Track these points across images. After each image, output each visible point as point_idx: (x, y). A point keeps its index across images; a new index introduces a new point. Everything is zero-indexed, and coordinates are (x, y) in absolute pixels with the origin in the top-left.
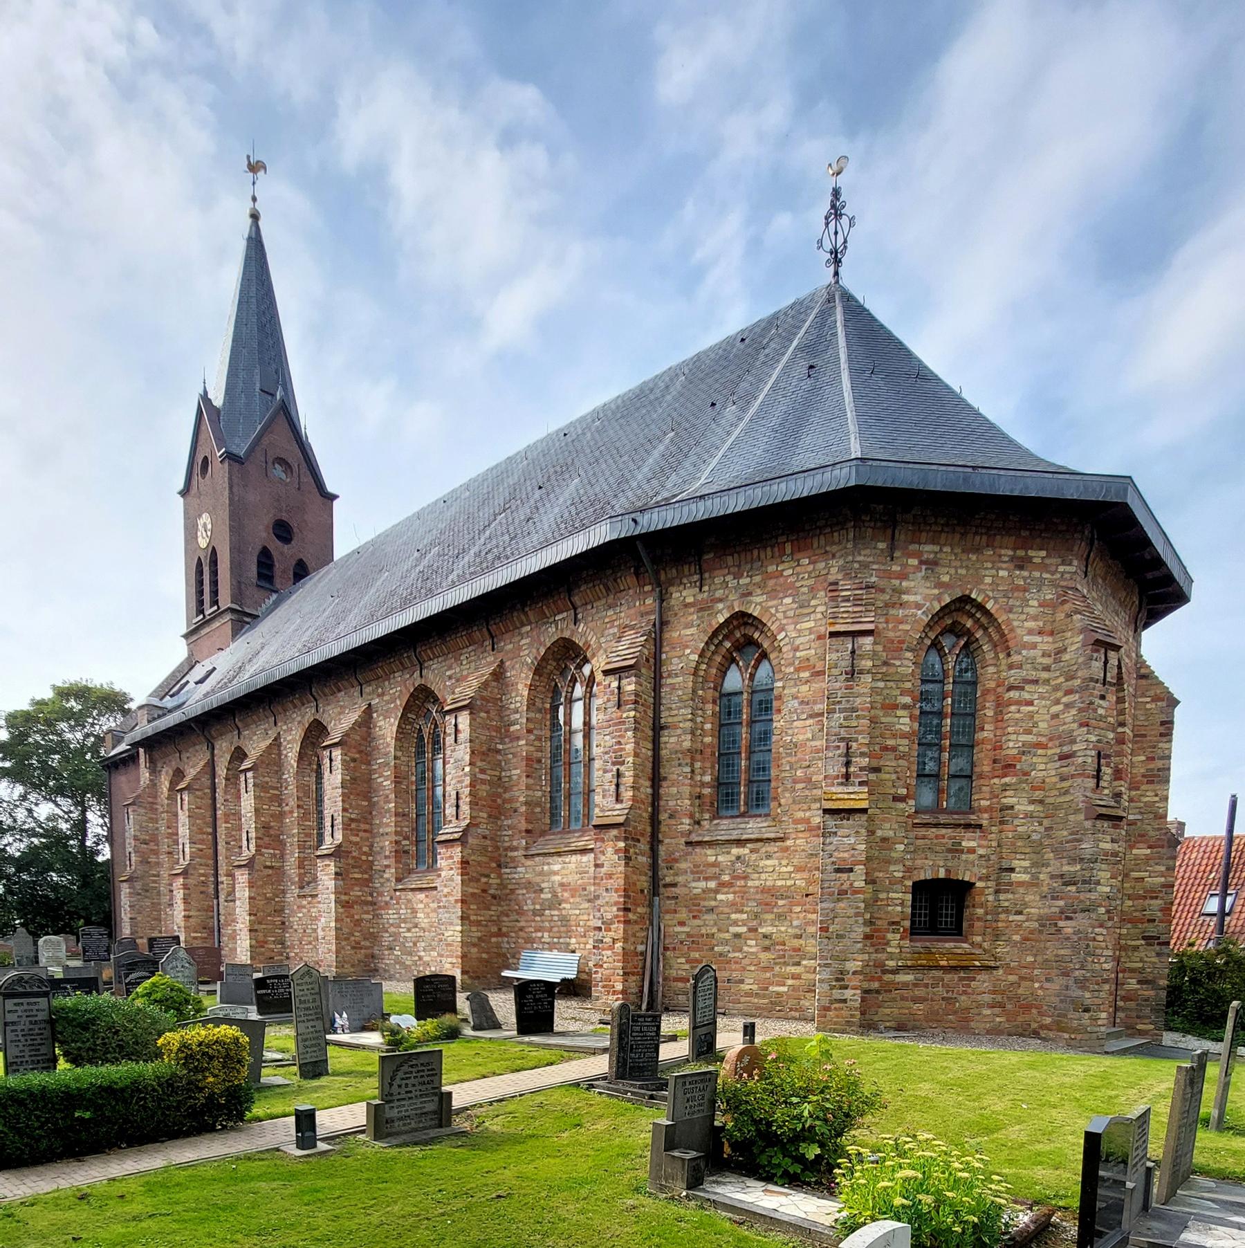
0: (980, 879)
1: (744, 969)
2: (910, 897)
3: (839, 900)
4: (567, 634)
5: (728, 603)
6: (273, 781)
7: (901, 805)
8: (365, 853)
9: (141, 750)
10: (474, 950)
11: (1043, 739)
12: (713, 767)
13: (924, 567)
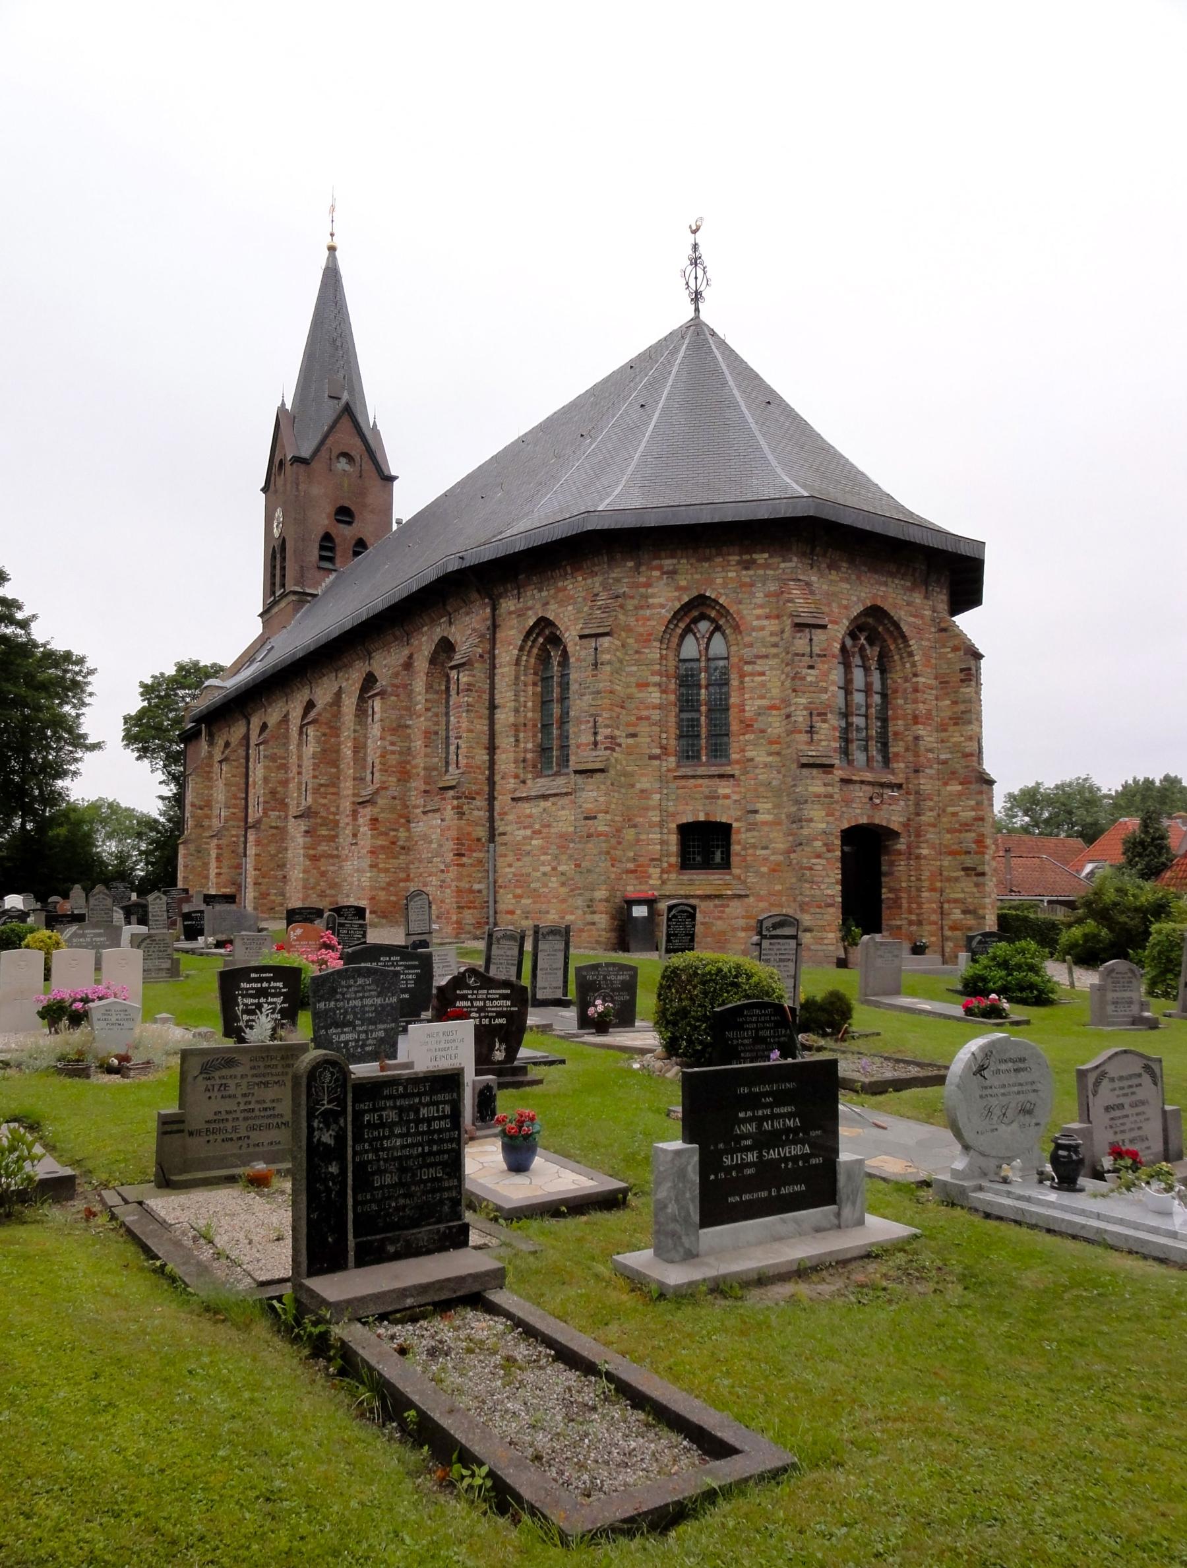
0: (736, 820)
1: (549, 902)
3: (587, 842)
6: (280, 752)
11: (777, 702)
12: (535, 736)
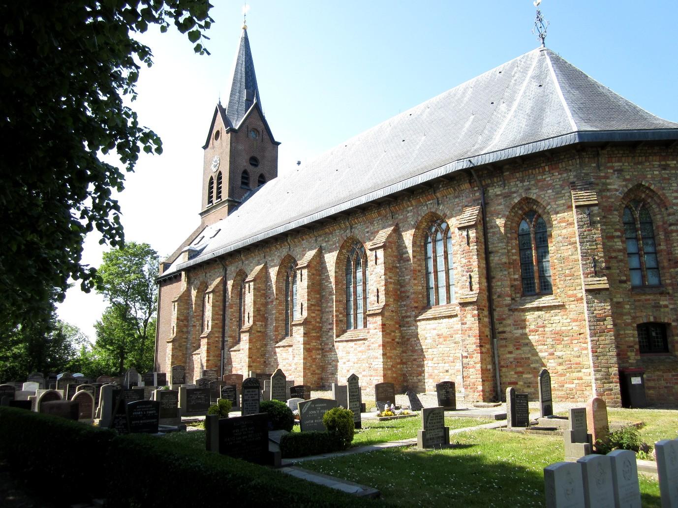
2: (636, 332)
4: (433, 210)
5: (519, 194)
7: (625, 285)
8: (318, 322)
9: (183, 273)
10: (389, 372)
13: (616, 173)
